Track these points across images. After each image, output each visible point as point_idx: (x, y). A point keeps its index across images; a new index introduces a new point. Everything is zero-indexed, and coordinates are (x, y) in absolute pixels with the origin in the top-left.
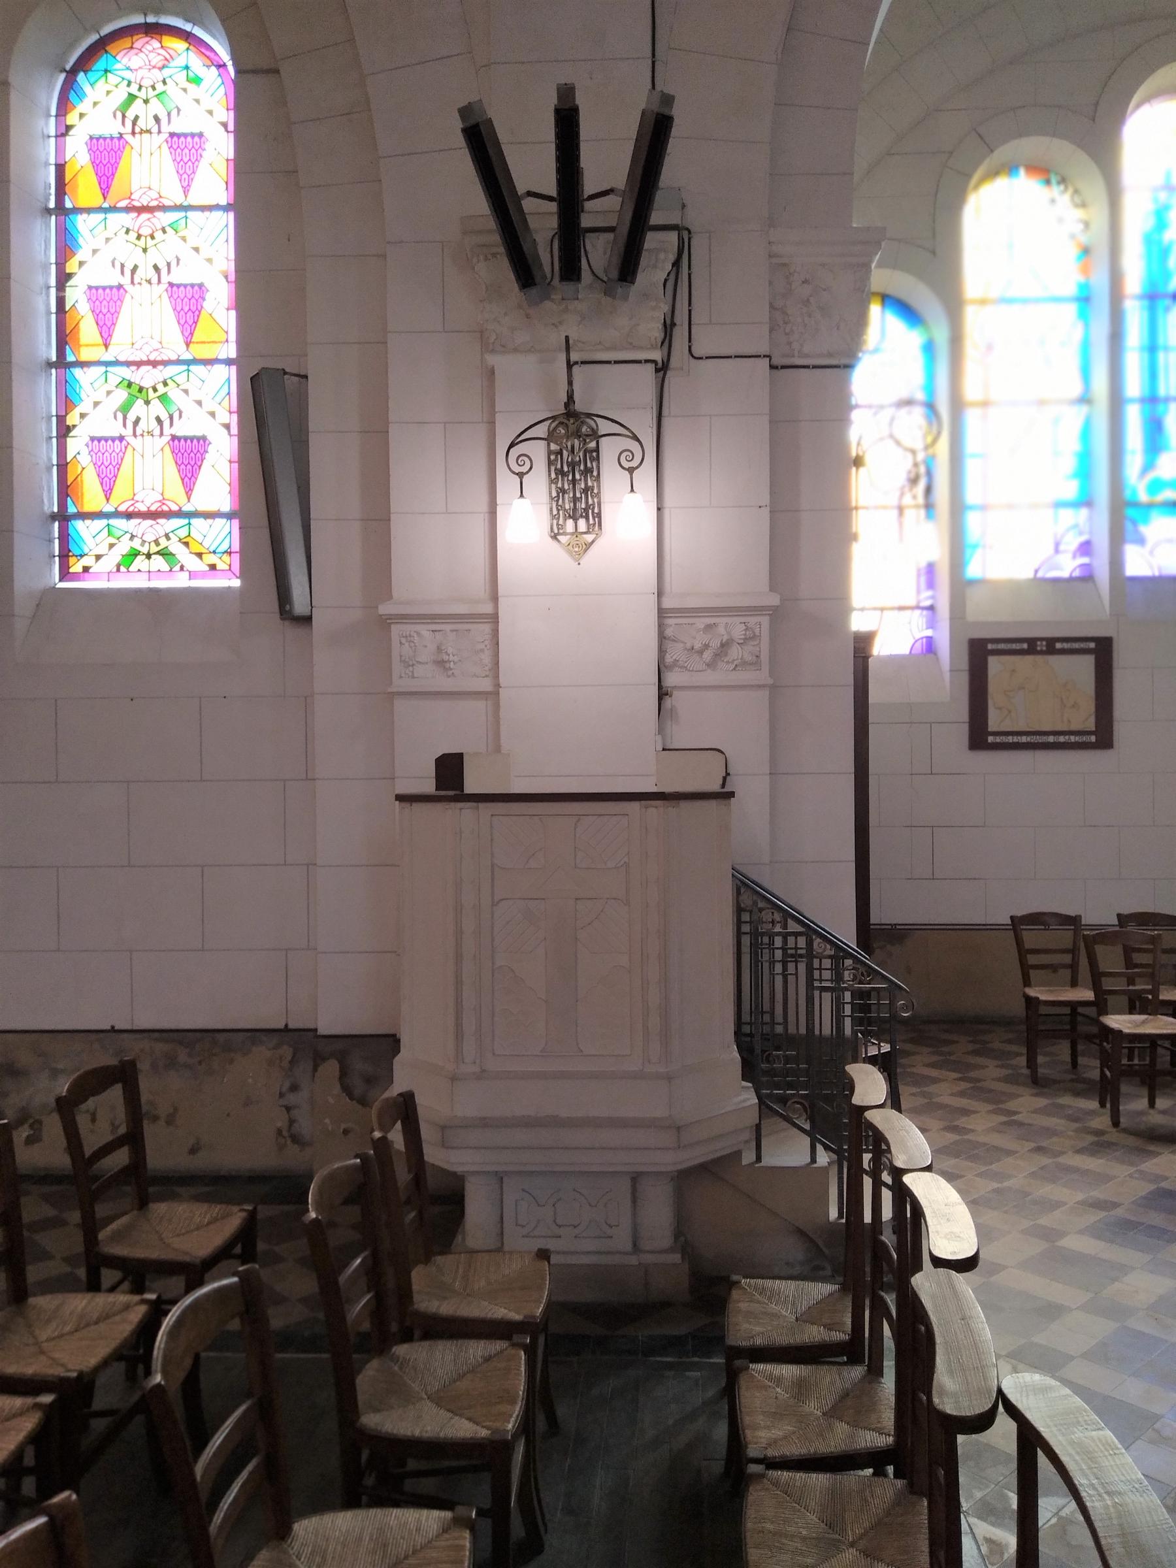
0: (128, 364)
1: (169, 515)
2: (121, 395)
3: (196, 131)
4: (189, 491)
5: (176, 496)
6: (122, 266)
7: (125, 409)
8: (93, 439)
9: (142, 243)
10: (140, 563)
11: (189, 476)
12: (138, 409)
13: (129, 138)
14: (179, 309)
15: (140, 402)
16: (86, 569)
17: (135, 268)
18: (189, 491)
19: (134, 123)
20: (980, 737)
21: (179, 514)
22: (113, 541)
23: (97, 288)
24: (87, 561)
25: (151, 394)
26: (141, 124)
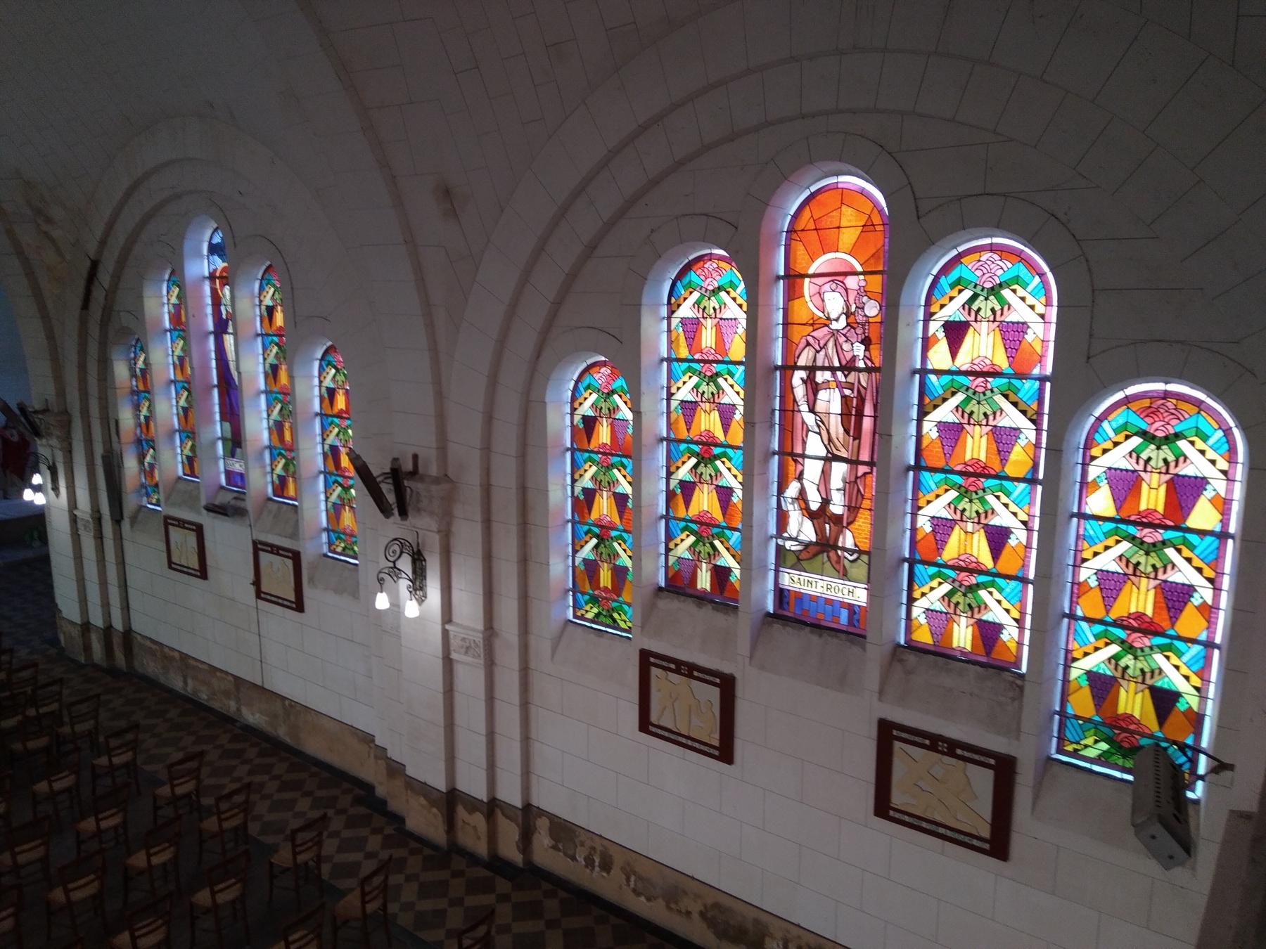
25: (1139, 652)
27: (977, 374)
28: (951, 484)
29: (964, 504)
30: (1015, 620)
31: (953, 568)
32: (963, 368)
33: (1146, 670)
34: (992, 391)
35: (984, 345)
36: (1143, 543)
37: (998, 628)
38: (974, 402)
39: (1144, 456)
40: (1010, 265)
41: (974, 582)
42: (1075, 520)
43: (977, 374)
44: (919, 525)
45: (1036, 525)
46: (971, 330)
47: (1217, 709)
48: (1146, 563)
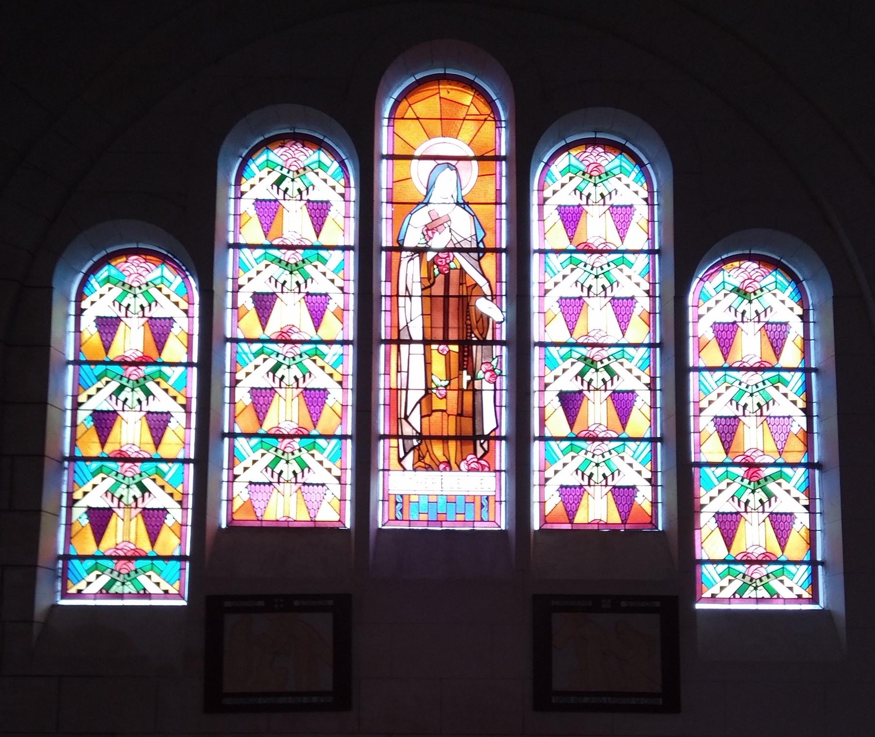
0: (585, 345)
1: (610, 252)
2: (580, 366)
3: (324, 292)
4: (622, 239)
5: (614, 241)
6: (582, 286)
7: (581, 374)
8: (562, 487)
9: (593, 180)
10: (750, 593)
11: (623, 322)
12: (590, 375)
13: (586, 393)
14: (617, 220)
15: (593, 370)
16: (713, 596)
17: (589, 195)
18: (622, 239)
19: (589, 384)
20: (215, 700)
21: (616, 251)
22: (574, 454)
23: (566, 298)
24: (82, 585)
25: (599, 365)
26: (594, 384)
27: (119, 558)
28: (112, 375)
29: (128, 300)
30: (182, 405)
31: (111, 558)
32: (107, 553)
33: (762, 403)
34: (136, 571)
35: (126, 531)
36: (287, 263)
37: (170, 321)
38: (124, 486)
39: (742, 403)
40: (152, 266)
41: (142, 374)
42: (231, 250)
43: (119, 558)
44: (74, 518)
45: (194, 408)
46: (122, 325)
47: (355, 397)
48: (291, 280)
